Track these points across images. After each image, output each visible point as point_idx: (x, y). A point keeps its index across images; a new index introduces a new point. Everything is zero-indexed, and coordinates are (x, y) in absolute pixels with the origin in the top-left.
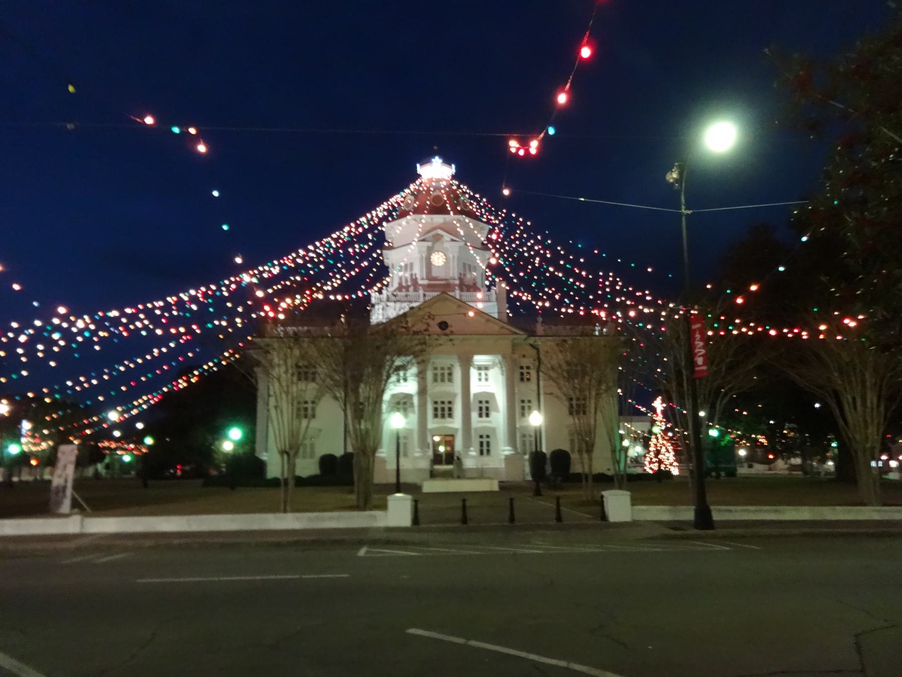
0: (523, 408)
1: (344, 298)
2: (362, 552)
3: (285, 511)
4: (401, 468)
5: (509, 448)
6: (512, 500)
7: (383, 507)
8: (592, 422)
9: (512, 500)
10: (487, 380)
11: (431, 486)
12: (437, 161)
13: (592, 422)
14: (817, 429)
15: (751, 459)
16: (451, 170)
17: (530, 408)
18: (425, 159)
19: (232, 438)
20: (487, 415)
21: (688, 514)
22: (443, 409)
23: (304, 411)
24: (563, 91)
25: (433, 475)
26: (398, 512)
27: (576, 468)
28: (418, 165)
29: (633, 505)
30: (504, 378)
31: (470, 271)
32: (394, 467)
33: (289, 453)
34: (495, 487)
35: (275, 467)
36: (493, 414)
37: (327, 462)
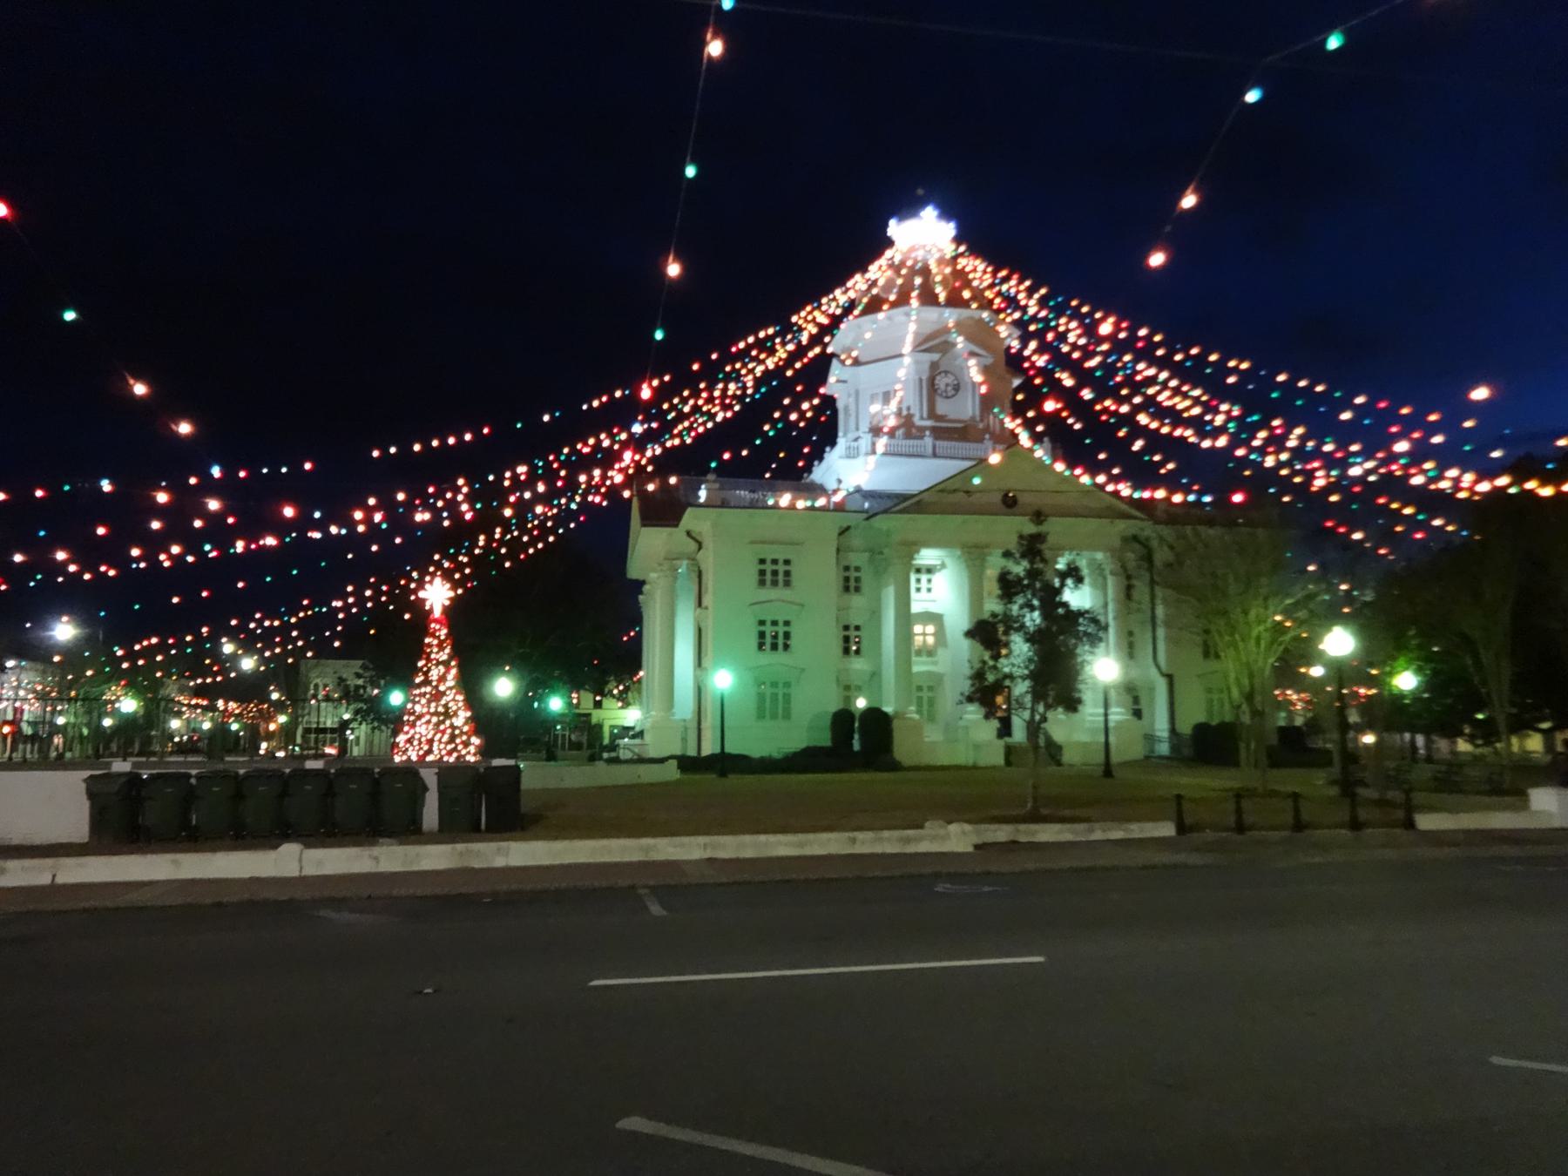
6: (689, 534)
9: (689, 534)
10: (929, 590)
12: (929, 213)
18: (907, 207)
22: (775, 573)
30: (963, 566)
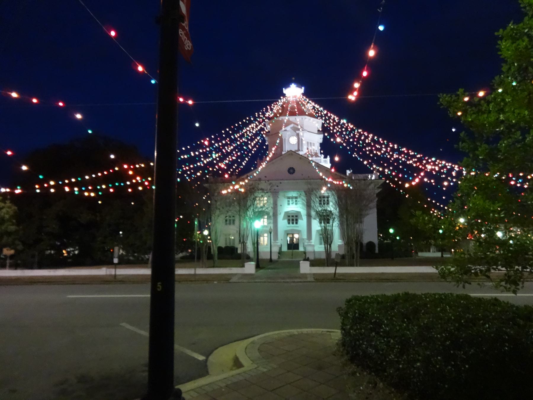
4: (259, 250)
5: (340, 241)
12: (293, 86)
16: (302, 90)
18: (287, 86)
20: (297, 223)
22: (230, 220)
24: (138, 66)
28: (284, 89)
31: (311, 146)
32: (269, 250)
36: (300, 221)
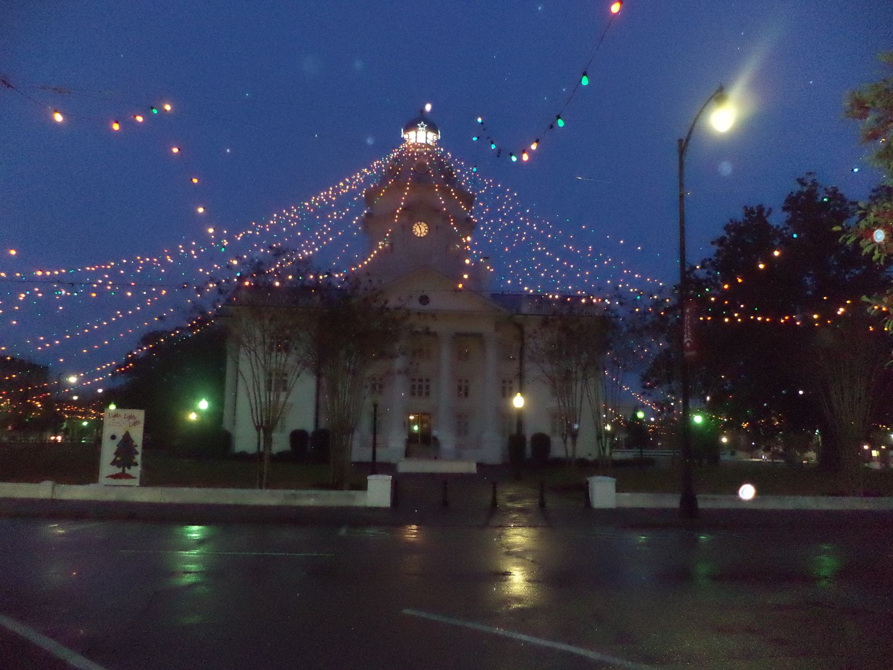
0: (504, 388)
1: (60, 272)
2: (343, 532)
3: (261, 488)
7: (362, 486)
8: (578, 406)
11: (405, 466)
13: (578, 406)
14: (801, 417)
15: (734, 446)
17: (511, 389)
19: (200, 409)
21: (672, 502)
23: (278, 382)
25: (408, 454)
26: (378, 492)
27: (558, 450)
29: (617, 491)
33: (266, 427)
34: (472, 468)
35: (246, 439)
37: (298, 437)
